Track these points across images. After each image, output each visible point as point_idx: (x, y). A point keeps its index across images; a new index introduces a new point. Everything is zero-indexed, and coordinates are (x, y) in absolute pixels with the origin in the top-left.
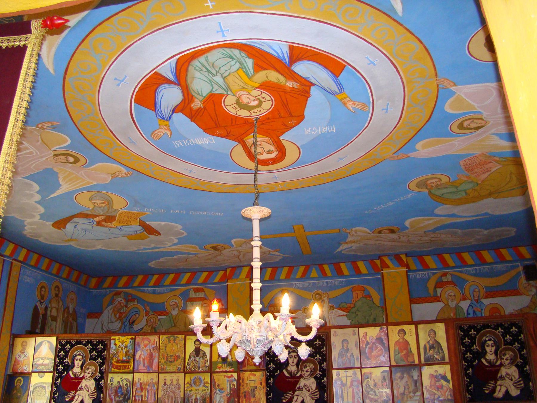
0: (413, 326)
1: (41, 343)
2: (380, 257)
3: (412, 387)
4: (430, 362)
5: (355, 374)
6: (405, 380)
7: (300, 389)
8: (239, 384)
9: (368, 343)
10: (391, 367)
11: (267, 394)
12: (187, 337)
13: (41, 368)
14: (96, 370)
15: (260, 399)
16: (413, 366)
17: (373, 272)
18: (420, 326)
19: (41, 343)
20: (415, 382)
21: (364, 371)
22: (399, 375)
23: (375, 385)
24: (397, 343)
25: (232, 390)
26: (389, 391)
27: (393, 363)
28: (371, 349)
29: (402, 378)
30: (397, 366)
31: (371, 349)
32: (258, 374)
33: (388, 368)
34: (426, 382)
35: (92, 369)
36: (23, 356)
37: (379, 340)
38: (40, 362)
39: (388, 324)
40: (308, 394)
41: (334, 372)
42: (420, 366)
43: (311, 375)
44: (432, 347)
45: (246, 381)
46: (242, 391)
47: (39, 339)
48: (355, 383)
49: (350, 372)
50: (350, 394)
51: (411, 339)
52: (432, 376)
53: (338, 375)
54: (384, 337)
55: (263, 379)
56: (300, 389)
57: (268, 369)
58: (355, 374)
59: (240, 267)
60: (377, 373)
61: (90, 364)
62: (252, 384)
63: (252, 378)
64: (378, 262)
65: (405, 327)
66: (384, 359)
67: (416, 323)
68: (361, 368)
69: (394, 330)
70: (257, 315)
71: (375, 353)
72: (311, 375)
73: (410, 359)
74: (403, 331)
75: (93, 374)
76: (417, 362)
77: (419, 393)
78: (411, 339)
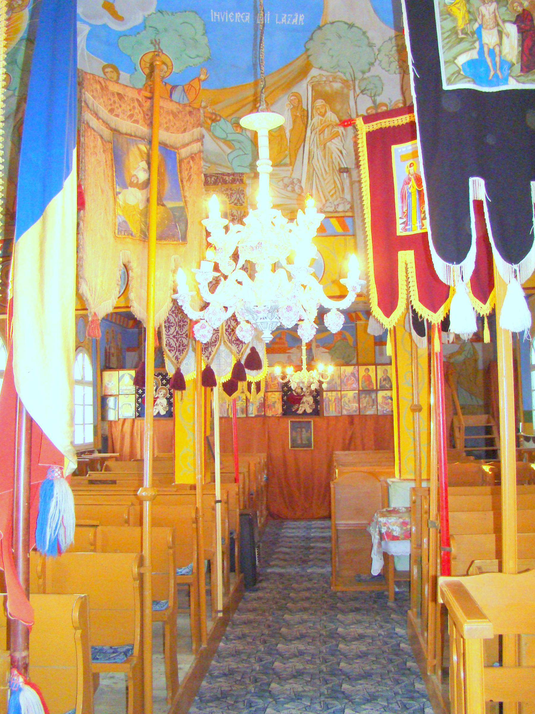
0: (374, 367)
1: (123, 375)
2: (355, 312)
3: (371, 403)
4: (383, 388)
5: (337, 394)
6: (367, 399)
7: (303, 403)
8: (265, 400)
9: (346, 376)
10: (359, 390)
11: (283, 406)
12: (358, 413)
13: (126, 392)
14: (167, 393)
15: (278, 409)
16: (373, 390)
17: (349, 321)
18: (378, 367)
19: (123, 375)
20: (373, 400)
21: (343, 392)
22: (363, 395)
23: (349, 401)
24: (364, 376)
25: (260, 403)
26: (357, 405)
27: (361, 389)
28: (348, 379)
29: (365, 398)
30: (363, 391)
31: (348, 379)
32: (277, 393)
33: (357, 392)
34: (380, 400)
35: (163, 391)
36: (110, 384)
37: (353, 374)
38: (125, 388)
39: (358, 364)
40: (308, 406)
41: (325, 393)
42: (377, 391)
43: (310, 395)
44: (385, 380)
45: (270, 398)
46: (267, 404)
47: (122, 372)
48: (337, 400)
49: (334, 393)
50: (334, 406)
51: (372, 375)
52: (383, 397)
53: (327, 395)
54: (356, 373)
55: (280, 397)
56: (303, 403)
57: (283, 391)
58: (337, 394)
59: (489, 439)
60: (351, 394)
61: (162, 388)
62: (273, 400)
63: (273, 396)
64: (354, 315)
65: (370, 367)
66: (355, 386)
67: (376, 365)
68: (341, 391)
69: (362, 369)
70: (465, 437)
71: (350, 382)
72: (310, 395)
73: (371, 387)
74: (368, 369)
75: (165, 395)
76: (375, 388)
77: (375, 407)
78: (372, 375)
